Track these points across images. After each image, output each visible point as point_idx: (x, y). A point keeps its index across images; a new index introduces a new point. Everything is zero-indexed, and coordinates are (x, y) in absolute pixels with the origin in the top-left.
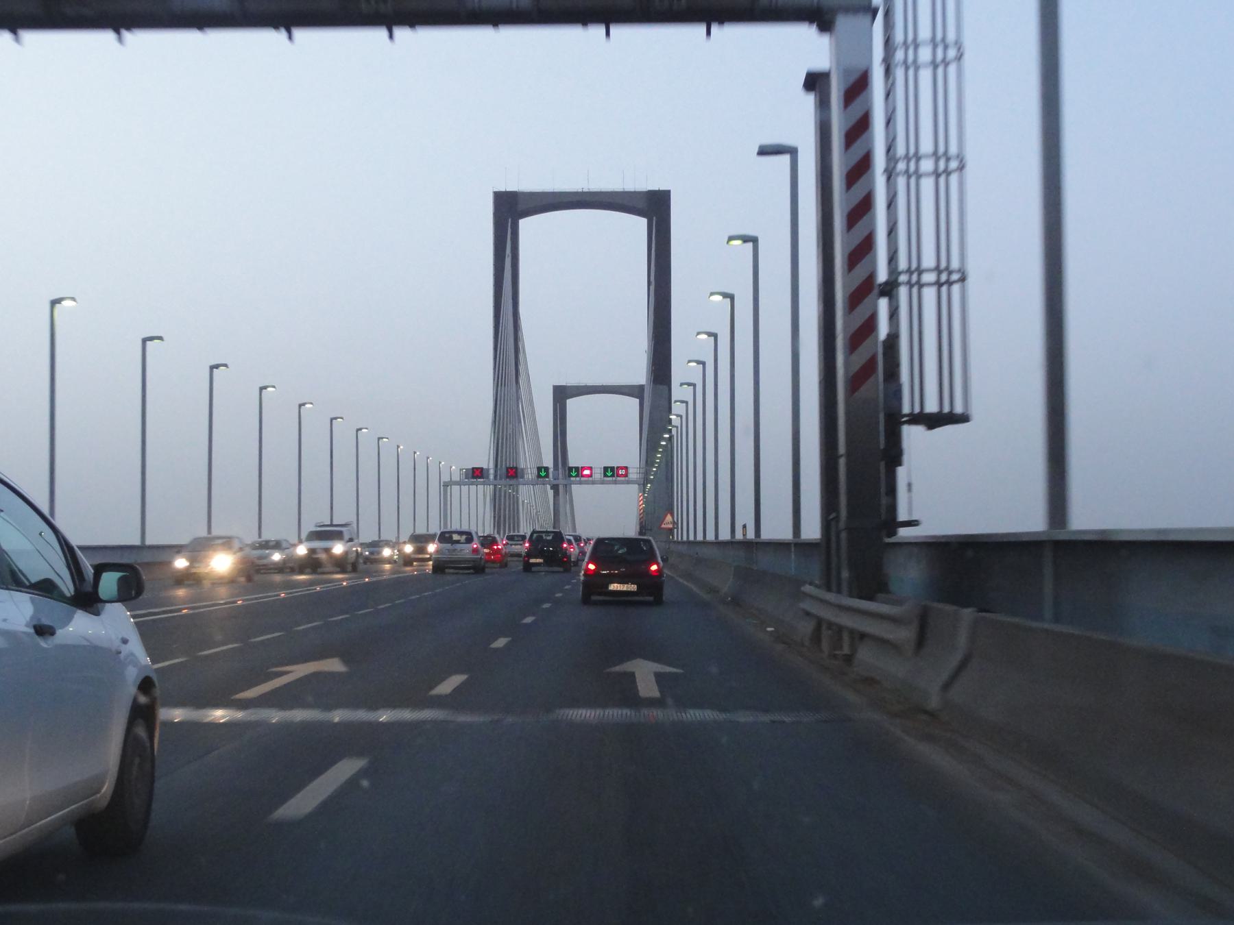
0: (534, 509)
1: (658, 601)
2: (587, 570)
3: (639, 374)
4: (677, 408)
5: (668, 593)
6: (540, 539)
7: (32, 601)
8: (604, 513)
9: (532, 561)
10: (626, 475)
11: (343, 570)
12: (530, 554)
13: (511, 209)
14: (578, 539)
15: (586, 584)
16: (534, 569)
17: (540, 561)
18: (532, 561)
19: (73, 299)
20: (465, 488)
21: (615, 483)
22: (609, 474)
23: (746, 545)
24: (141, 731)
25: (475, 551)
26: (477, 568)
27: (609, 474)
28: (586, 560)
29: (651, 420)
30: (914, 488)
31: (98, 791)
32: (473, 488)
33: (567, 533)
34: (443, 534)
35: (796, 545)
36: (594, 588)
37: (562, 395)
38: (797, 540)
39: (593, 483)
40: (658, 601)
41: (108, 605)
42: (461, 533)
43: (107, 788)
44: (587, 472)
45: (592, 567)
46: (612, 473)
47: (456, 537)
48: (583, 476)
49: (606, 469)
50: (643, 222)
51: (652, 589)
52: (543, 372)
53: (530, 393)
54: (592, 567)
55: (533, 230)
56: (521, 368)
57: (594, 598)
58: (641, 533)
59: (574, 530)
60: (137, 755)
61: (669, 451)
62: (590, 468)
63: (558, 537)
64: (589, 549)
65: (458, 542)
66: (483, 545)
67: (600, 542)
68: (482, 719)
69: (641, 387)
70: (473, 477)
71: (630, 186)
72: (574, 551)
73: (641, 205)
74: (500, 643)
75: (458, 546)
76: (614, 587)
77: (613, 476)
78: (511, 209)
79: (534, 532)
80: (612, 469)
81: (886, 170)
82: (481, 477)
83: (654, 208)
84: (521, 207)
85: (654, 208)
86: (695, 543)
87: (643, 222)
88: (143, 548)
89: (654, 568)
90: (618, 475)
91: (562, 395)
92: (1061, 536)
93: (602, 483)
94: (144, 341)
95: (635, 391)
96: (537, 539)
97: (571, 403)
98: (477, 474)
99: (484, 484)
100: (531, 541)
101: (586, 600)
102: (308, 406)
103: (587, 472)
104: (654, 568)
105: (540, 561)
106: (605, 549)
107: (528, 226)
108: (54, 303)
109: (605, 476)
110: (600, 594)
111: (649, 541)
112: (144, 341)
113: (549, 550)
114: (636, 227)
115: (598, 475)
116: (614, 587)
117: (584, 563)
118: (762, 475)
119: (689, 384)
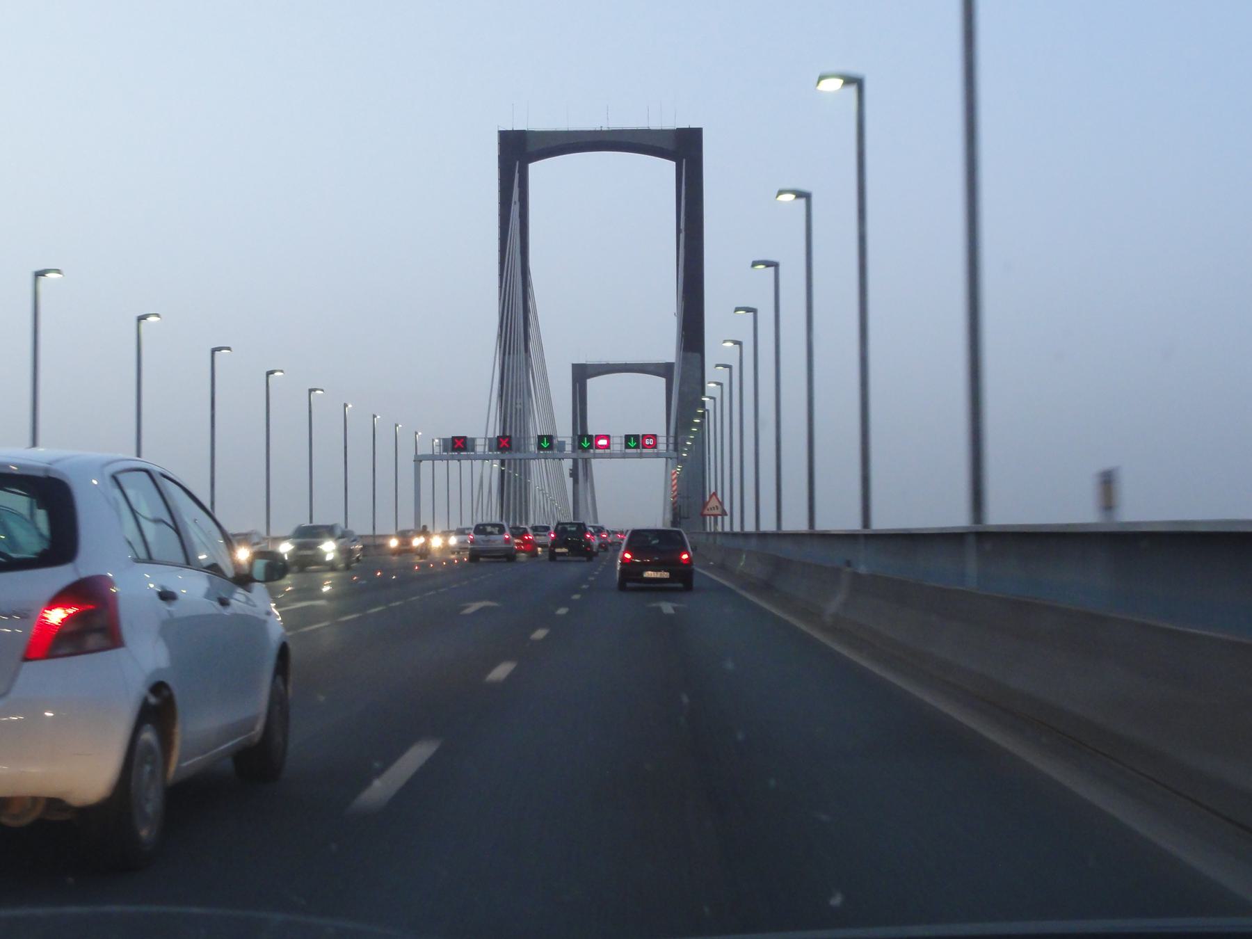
0: (548, 495)
2: (624, 559)
3: (667, 349)
4: (710, 387)
6: (564, 531)
7: (210, 579)
8: (631, 497)
9: (558, 550)
10: (654, 446)
11: (453, 553)
12: (555, 544)
13: (519, 151)
14: (599, 530)
16: (559, 558)
17: (564, 550)
18: (558, 550)
19: (157, 315)
20: (440, 465)
21: (641, 456)
22: (632, 444)
24: (148, 736)
25: (507, 541)
26: (509, 556)
27: (632, 444)
29: (682, 396)
31: (253, 729)
32: (454, 464)
33: (589, 523)
34: (478, 526)
35: (867, 536)
36: (630, 574)
37: (582, 374)
38: (867, 532)
39: (611, 456)
41: (257, 584)
42: (493, 525)
43: (259, 727)
44: (603, 442)
45: (628, 556)
46: (637, 443)
47: (489, 529)
48: (598, 447)
49: (628, 438)
50: (672, 165)
51: (683, 578)
52: (558, 345)
53: (543, 361)
54: (628, 556)
56: (532, 331)
57: (628, 585)
58: (674, 523)
59: (596, 521)
60: (279, 706)
61: (701, 442)
62: (607, 437)
63: (582, 528)
65: (491, 533)
66: (514, 535)
69: (669, 367)
70: (454, 450)
71: (656, 124)
74: (540, 634)
75: (492, 537)
76: (649, 574)
77: (637, 447)
78: (519, 151)
79: (559, 524)
80: (636, 437)
82: (465, 449)
83: (683, 148)
85: (683, 148)
86: (735, 535)
87: (672, 165)
88: (374, 536)
89: (685, 556)
90: (645, 447)
91: (582, 374)
92: (980, 528)
93: (624, 456)
95: (664, 370)
96: (561, 529)
97: (592, 384)
98: (459, 445)
99: (468, 458)
100: (555, 532)
101: (622, 587)
102: (152, 319)
103: (603, 442)
104: (685, 556)
105: (564, 550)
106: (639, 539)
107: (539, 171)
108: (141, 318)
109: (627, 447)
110: (635, 581)
111: (679, 533)
113: (574, 540)
114: (661, 173)
115: (617, 446)
116: (649, 574)
117: (621, 553)
119: (725, 366)
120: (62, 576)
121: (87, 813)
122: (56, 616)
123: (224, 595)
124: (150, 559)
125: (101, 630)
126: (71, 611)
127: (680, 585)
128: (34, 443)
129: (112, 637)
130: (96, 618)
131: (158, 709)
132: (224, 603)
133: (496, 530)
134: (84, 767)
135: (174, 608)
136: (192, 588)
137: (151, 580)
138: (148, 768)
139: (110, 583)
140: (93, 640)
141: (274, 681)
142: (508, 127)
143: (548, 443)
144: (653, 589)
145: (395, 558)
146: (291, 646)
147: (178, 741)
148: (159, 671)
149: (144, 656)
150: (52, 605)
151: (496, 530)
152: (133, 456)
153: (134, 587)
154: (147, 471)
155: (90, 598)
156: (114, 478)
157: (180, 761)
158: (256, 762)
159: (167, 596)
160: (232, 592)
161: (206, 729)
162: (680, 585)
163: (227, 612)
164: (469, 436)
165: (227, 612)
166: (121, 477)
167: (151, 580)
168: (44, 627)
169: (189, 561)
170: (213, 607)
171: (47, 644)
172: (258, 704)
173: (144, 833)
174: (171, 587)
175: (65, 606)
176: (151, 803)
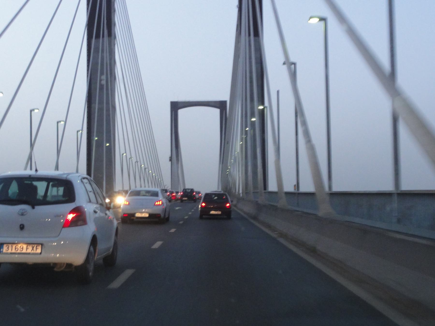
2: (202, 206)
9: (184, 199)
12: (182, 196)
13: (176, 107)
17: (186, 199)
18: (184, 199)
23: (217, 210)
24: (92, 249)
28: (202, 201)
36: (205, 212)
43: (111, 250)
51: (227, 214)
54: (204, 204)
55: (181, 112)
57: (204, 216)
64: (203, 196)
67: (207, 195)
68: (12, 249)
72: (197, 196)
78: (176, 107)
89: (228, 205)
101: (201, 217)
102: (36, 111)
104: (228, 205)
106: (208, 197)
116: (213, 212)
118: (162, 216)
120: (72, 206)
121: (78, 268)
122: (70, 217)
126: (74, 215)
127: (225, 217)
130: (80, 217)
131: (94, 241)
133: (57, 192)
134: (78, 257)
135: (97, 215)
139: (84, 208)
140: (79, 223)
142: (176, 100)
146: (98, 236)
147: (97, 251)
149: (90, 229)
150: (70, 213)
151: (57, 192)
153: (89, 208)
155: (78, 211)
157: (98, 256)
161: (104, 246)
162: (225, 217)
164: (196, 189)
168: (67, 221)
171: (68, 224)
175: (73, 214)
176: (91, 267)
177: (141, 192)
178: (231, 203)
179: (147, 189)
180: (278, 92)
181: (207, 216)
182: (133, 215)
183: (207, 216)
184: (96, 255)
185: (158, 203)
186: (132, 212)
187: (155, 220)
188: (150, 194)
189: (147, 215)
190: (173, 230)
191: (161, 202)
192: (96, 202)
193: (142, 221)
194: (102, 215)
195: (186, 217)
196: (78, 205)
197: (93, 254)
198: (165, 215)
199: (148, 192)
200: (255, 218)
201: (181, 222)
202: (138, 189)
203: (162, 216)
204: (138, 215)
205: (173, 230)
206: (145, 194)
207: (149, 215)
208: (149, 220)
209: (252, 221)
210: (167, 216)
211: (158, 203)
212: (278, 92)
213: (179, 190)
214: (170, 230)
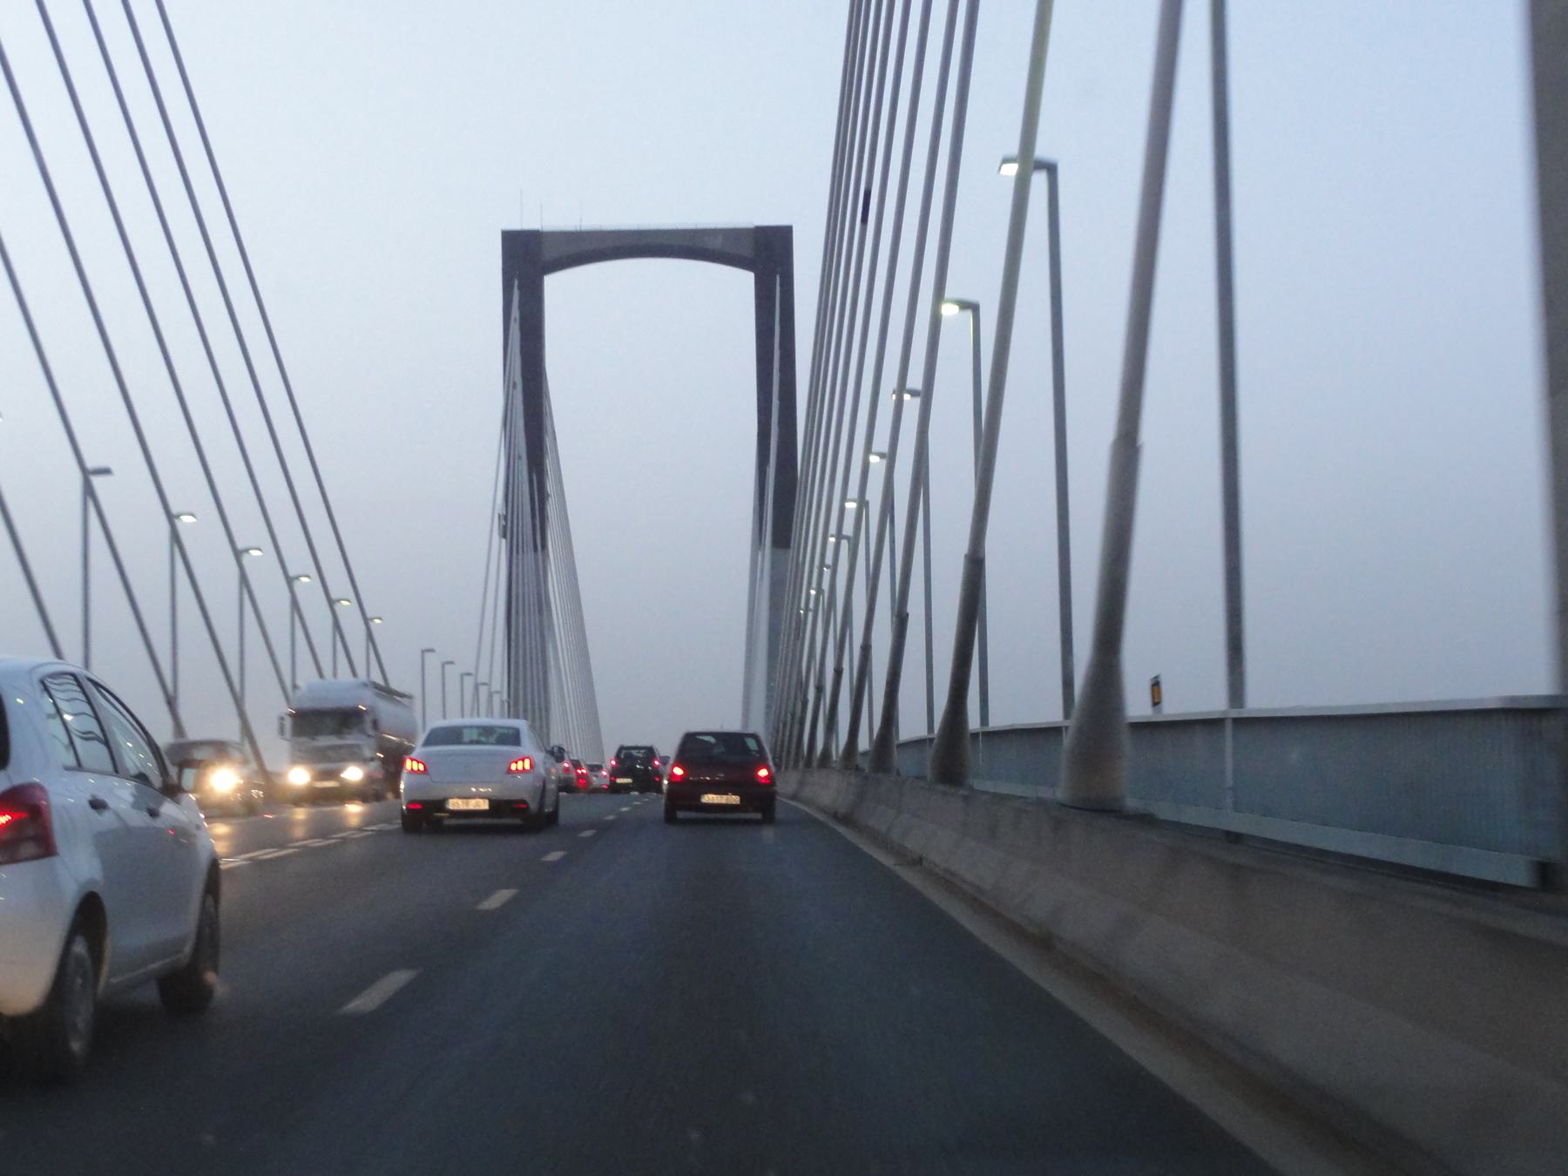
1: (769, 818)
2: (672, 776)
5: (780, 813)
9: (619, 781)
12: (615, 773)
13: (530, 260)
15: (672, 793)
18: (619, 781)
24: (80, 948)
30: (1164, 687)
36: (682, 798)
38: (1235, 713)
40: (769, 818)
43: (188, 949)
45: (678, 771)
51: (761, 800)
54: (678, 771)
55: (558, 287)
56: (550, 487)
57: (681, 815)
73: (747, 251)
76: (709, 798)
78: (530, 260)
81: (338, 732)
84: (549, 253)
89: (763, 773)
94: (423, 652)
101: (670, 818)
104: (763, 773)
110: (689, 808)
112: (423, 652)
116: (709, 798)
123: (152, 806)
124: (79, 766)
125: (35, 839)
127: (758, 816)
128: (444, 717)
129: (45, 847)
131: (89, 915)
132: (153, 814)
135: (106, 819)
136: (121, 794)
137: (91, 784)
138: (79, 981)
141: (203, 903)
143: (914, 393)
144: (723, 822)
145: (300, 814)
146: (109, 904)
147: (108, 954)
148: (92, 881)
149: (78, 866)
152: (52, 658)
153: (65, 795)
154: (73, 675)
156: (42, 682)
158: (182, 990)
159: (97, 805)
160: (160, 804)
161: (136, 938)
162: (758, 816)
163: (158, 823)
165: (158, 823)
166: (48, 682)
167: (91, 784)
169: (117, 769)
170: (139, 819)
172: (188, 923)
173: (76, 1046)
174: (101, 796)
176: (82, 1016)
177: (466, 732)
178: (773, 769)
179: (484, 720)
180: (1156, 685)
181: (693, 815)
182: (440, 805)
183: (693, 815)
184: (105, 969)
185: (520, 765)
186: (434, 794)
187: (513, 818)
188: (492, 739)
189: (484, 805)
190: (554, 856)
191: (527, 762)
192: (110, 768)
193: (469, 825)
194: (139, 819)
195: (611, 817)
196: (18, 781)
197: (88, 963)
198: (541, 805)
199: (487, 731)
200: (847, 820)
201: (588, 833)
202: (454, 720)
203: (533, 806)
204: (455, 804)
205: (554, 856)
206: (475, 737)
207: (491, 801)
208: (489, 821)
209: (841, 830)
210: (547, 810)
211: (520, 765)
212: (1156, 685)
213: (207, 716)
214: (546, 853)
